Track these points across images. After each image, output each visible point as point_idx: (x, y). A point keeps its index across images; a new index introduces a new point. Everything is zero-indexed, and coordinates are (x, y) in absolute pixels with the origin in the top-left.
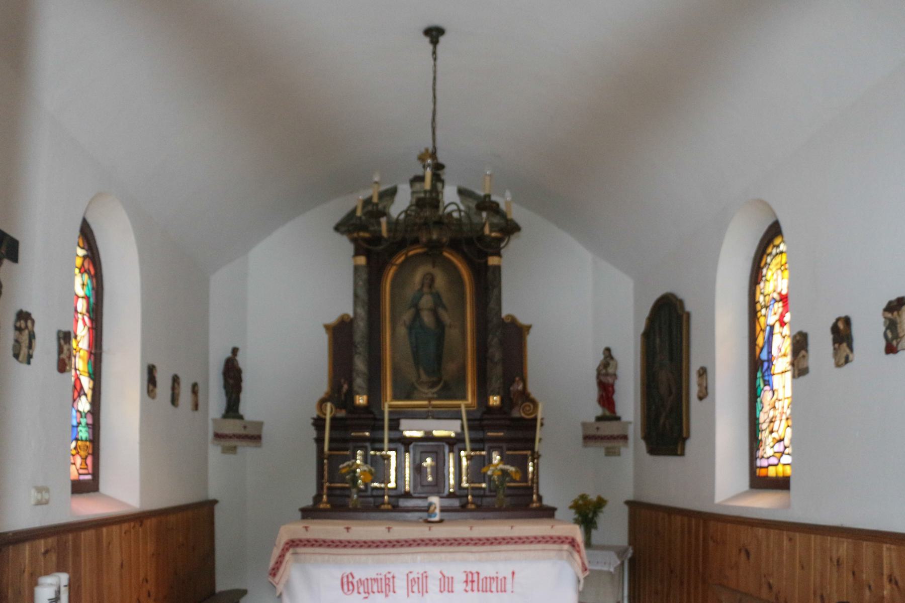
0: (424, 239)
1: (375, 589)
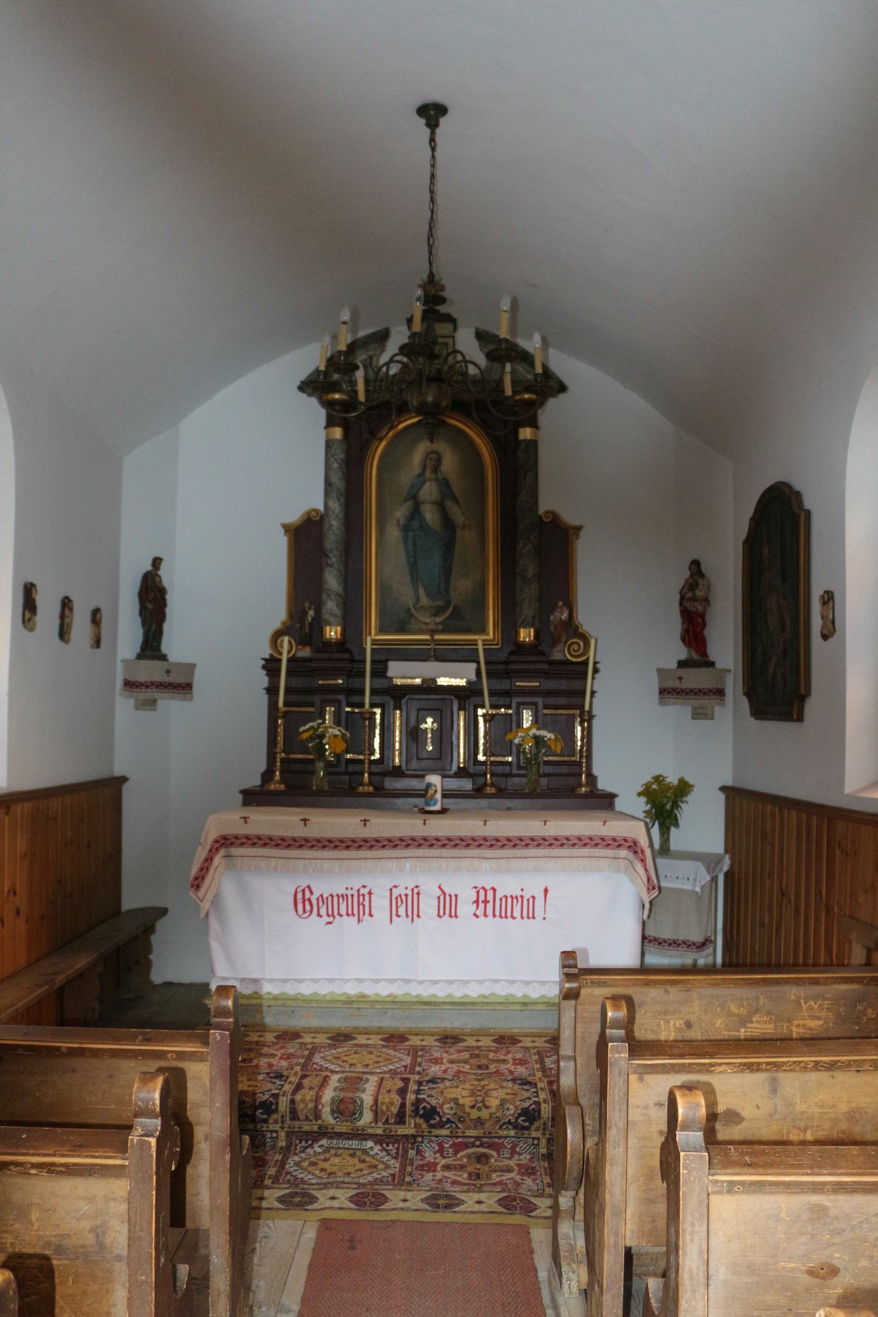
0: (414, 401)
1: (343, 910)
